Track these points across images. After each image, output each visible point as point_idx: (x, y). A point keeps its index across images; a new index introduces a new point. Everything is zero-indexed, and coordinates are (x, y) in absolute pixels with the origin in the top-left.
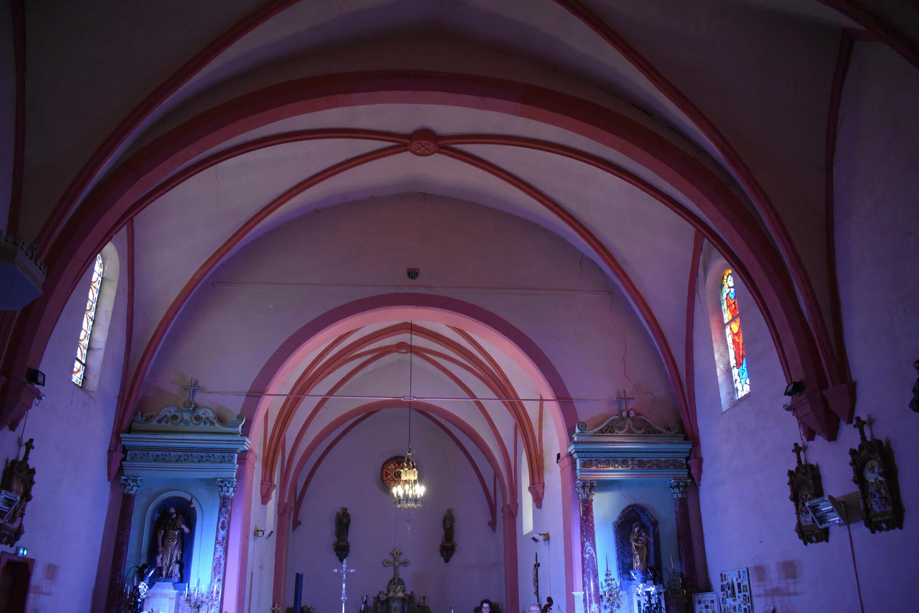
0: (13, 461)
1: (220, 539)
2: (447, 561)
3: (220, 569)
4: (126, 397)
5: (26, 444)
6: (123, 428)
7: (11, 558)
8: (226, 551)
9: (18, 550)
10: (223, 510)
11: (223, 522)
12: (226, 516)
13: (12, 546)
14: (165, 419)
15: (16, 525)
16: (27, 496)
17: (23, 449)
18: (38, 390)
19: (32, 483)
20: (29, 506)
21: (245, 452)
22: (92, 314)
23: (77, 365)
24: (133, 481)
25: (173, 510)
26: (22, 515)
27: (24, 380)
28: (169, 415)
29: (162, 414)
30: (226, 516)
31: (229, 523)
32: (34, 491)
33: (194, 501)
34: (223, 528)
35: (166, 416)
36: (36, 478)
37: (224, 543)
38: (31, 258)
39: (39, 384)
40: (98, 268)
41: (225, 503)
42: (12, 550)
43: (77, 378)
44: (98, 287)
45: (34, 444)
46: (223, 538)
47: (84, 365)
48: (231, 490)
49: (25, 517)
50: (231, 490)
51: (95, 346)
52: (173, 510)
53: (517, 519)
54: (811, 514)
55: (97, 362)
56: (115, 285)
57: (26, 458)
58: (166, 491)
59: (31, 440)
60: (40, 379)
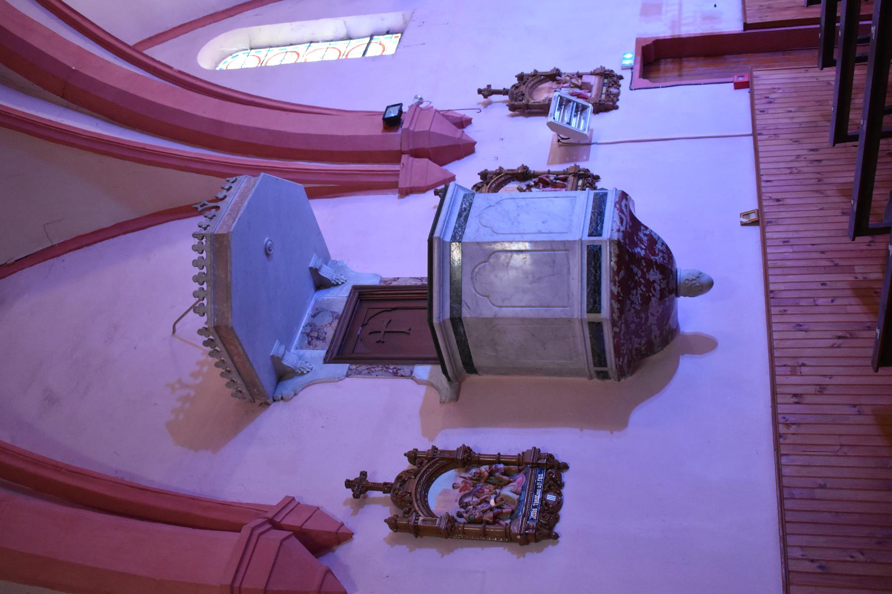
0: (510, 109)
2: (385, 521)
5: (485, 97)
7: (637, 73)
9: (625, 68)
13: (621, 78)
15: (594, 81)
16: (554, 76)
17: (494, 98)
18: (410, 107)
19: (535, 74)
20: (567, 69)
22: (301, 49)
23: (375, 50)
26: (580, 76)
27: (399, 132)
32: (545, 68)
36: (528, 71)
38: (217, 208)
39: (401, 112)
40: (234, 63)
42: (627, 75)
43: (390, 43)
44: (264, 51)
45: (483, 86)
47: (371, 37)
49: (581, 71)
51: (342, 33)
55: (363, 23)
56: (255, 29)
57: (504, 92)
59: (480, 92)
60: (393, 113)
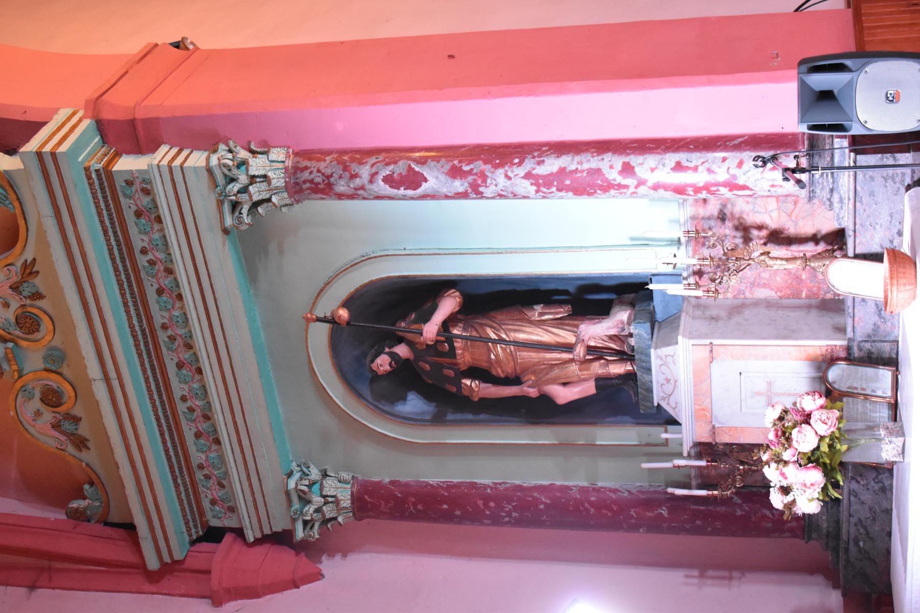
1: (459, 185)
3: (581, 164)
4: (31, 561)
6: (124, 554)
8: (504, 154)
10: (341, 187)
11: (388, 180)
12: (365, 172)
14: (67, 426)
21: (102, 127)
24: (305, 500)
25: (383, 363)
28: (48, 416)
29: (50, 440)
30: (365, 172)
31: (391, 154)
33: (323, 310)
34: (413, 180)
35: (56, 426)
37: (477, 163)
41: (315, 178)
46: (456, 173)
48: (257, 165)
50: (257, 165)
52: (383, 363)
53: (704, 78)
54: (719, 247)
58: (321, 391)
